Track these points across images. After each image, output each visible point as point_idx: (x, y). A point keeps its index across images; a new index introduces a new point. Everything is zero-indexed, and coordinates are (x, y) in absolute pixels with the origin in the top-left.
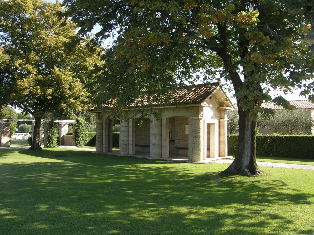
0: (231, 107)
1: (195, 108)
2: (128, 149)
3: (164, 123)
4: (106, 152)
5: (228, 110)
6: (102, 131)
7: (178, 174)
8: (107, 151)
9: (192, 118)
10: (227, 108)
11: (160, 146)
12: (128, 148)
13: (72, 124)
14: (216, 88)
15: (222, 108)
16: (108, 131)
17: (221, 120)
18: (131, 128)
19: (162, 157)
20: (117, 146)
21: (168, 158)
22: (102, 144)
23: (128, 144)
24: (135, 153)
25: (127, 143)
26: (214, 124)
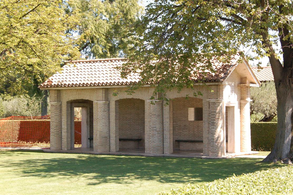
0: (255, 83)
1: (213, 87)
2: (108, 144)
3: (113, 106)
4: (68, 150)
5: (252, 88)
6: (61, 118)
7: (94, 174)
8: (70, 148)
9: (97, 102)
10: (251, 85)
11: (162, 139)
12: (108, 142)
13: (222, 109)
14: (200, 66)
15: (244, 85)
16: (70, 118)
17: (242, 102)
18: (113, 114)
19: (110, 151)
20: (79, 142)
21: (172, 154)
22: (61, 138)
23: (108, 137)
24: (118, 149)
25: (108, 135)
26: (234, 107)
